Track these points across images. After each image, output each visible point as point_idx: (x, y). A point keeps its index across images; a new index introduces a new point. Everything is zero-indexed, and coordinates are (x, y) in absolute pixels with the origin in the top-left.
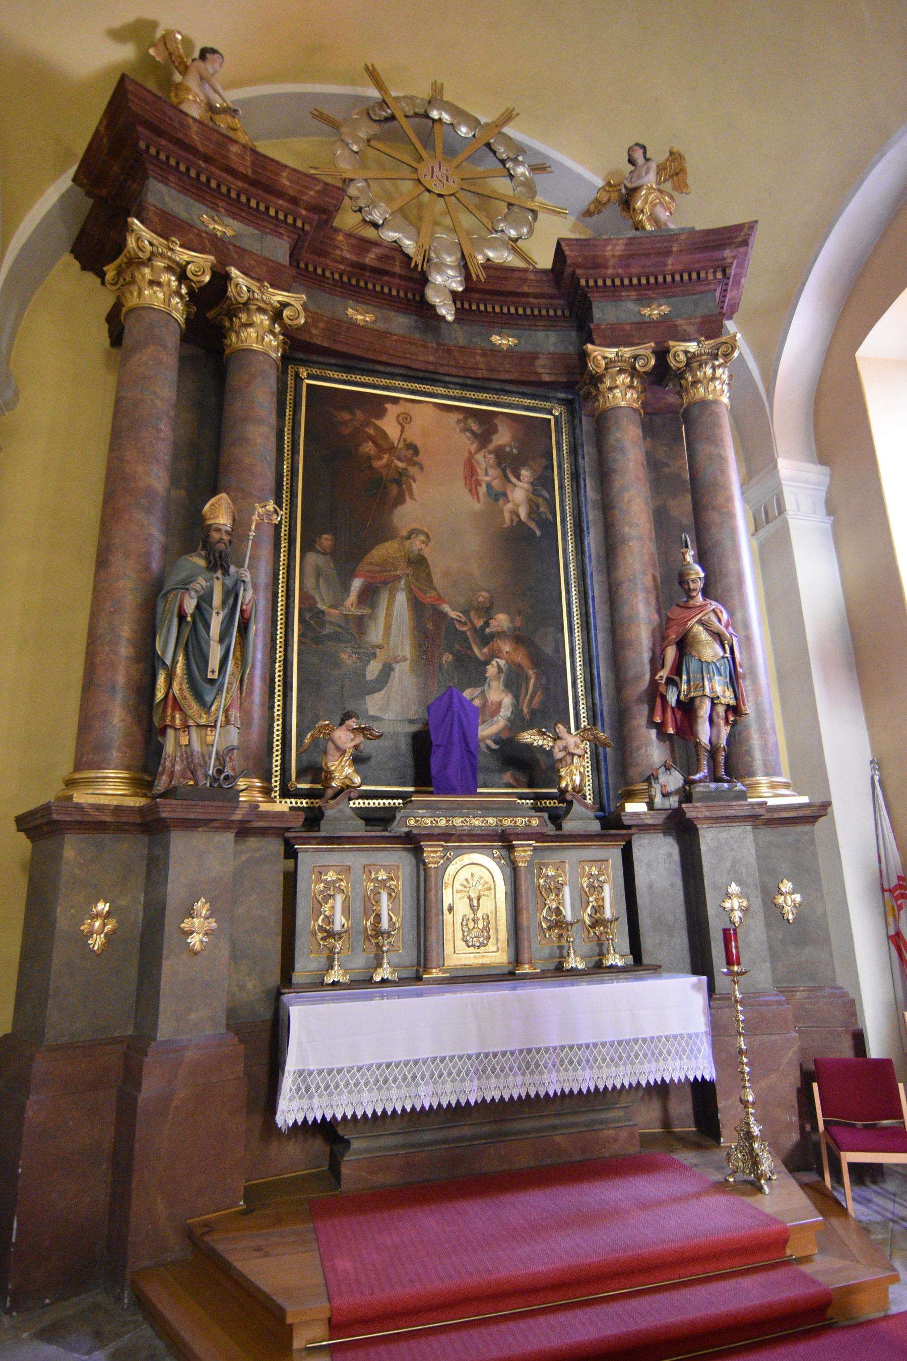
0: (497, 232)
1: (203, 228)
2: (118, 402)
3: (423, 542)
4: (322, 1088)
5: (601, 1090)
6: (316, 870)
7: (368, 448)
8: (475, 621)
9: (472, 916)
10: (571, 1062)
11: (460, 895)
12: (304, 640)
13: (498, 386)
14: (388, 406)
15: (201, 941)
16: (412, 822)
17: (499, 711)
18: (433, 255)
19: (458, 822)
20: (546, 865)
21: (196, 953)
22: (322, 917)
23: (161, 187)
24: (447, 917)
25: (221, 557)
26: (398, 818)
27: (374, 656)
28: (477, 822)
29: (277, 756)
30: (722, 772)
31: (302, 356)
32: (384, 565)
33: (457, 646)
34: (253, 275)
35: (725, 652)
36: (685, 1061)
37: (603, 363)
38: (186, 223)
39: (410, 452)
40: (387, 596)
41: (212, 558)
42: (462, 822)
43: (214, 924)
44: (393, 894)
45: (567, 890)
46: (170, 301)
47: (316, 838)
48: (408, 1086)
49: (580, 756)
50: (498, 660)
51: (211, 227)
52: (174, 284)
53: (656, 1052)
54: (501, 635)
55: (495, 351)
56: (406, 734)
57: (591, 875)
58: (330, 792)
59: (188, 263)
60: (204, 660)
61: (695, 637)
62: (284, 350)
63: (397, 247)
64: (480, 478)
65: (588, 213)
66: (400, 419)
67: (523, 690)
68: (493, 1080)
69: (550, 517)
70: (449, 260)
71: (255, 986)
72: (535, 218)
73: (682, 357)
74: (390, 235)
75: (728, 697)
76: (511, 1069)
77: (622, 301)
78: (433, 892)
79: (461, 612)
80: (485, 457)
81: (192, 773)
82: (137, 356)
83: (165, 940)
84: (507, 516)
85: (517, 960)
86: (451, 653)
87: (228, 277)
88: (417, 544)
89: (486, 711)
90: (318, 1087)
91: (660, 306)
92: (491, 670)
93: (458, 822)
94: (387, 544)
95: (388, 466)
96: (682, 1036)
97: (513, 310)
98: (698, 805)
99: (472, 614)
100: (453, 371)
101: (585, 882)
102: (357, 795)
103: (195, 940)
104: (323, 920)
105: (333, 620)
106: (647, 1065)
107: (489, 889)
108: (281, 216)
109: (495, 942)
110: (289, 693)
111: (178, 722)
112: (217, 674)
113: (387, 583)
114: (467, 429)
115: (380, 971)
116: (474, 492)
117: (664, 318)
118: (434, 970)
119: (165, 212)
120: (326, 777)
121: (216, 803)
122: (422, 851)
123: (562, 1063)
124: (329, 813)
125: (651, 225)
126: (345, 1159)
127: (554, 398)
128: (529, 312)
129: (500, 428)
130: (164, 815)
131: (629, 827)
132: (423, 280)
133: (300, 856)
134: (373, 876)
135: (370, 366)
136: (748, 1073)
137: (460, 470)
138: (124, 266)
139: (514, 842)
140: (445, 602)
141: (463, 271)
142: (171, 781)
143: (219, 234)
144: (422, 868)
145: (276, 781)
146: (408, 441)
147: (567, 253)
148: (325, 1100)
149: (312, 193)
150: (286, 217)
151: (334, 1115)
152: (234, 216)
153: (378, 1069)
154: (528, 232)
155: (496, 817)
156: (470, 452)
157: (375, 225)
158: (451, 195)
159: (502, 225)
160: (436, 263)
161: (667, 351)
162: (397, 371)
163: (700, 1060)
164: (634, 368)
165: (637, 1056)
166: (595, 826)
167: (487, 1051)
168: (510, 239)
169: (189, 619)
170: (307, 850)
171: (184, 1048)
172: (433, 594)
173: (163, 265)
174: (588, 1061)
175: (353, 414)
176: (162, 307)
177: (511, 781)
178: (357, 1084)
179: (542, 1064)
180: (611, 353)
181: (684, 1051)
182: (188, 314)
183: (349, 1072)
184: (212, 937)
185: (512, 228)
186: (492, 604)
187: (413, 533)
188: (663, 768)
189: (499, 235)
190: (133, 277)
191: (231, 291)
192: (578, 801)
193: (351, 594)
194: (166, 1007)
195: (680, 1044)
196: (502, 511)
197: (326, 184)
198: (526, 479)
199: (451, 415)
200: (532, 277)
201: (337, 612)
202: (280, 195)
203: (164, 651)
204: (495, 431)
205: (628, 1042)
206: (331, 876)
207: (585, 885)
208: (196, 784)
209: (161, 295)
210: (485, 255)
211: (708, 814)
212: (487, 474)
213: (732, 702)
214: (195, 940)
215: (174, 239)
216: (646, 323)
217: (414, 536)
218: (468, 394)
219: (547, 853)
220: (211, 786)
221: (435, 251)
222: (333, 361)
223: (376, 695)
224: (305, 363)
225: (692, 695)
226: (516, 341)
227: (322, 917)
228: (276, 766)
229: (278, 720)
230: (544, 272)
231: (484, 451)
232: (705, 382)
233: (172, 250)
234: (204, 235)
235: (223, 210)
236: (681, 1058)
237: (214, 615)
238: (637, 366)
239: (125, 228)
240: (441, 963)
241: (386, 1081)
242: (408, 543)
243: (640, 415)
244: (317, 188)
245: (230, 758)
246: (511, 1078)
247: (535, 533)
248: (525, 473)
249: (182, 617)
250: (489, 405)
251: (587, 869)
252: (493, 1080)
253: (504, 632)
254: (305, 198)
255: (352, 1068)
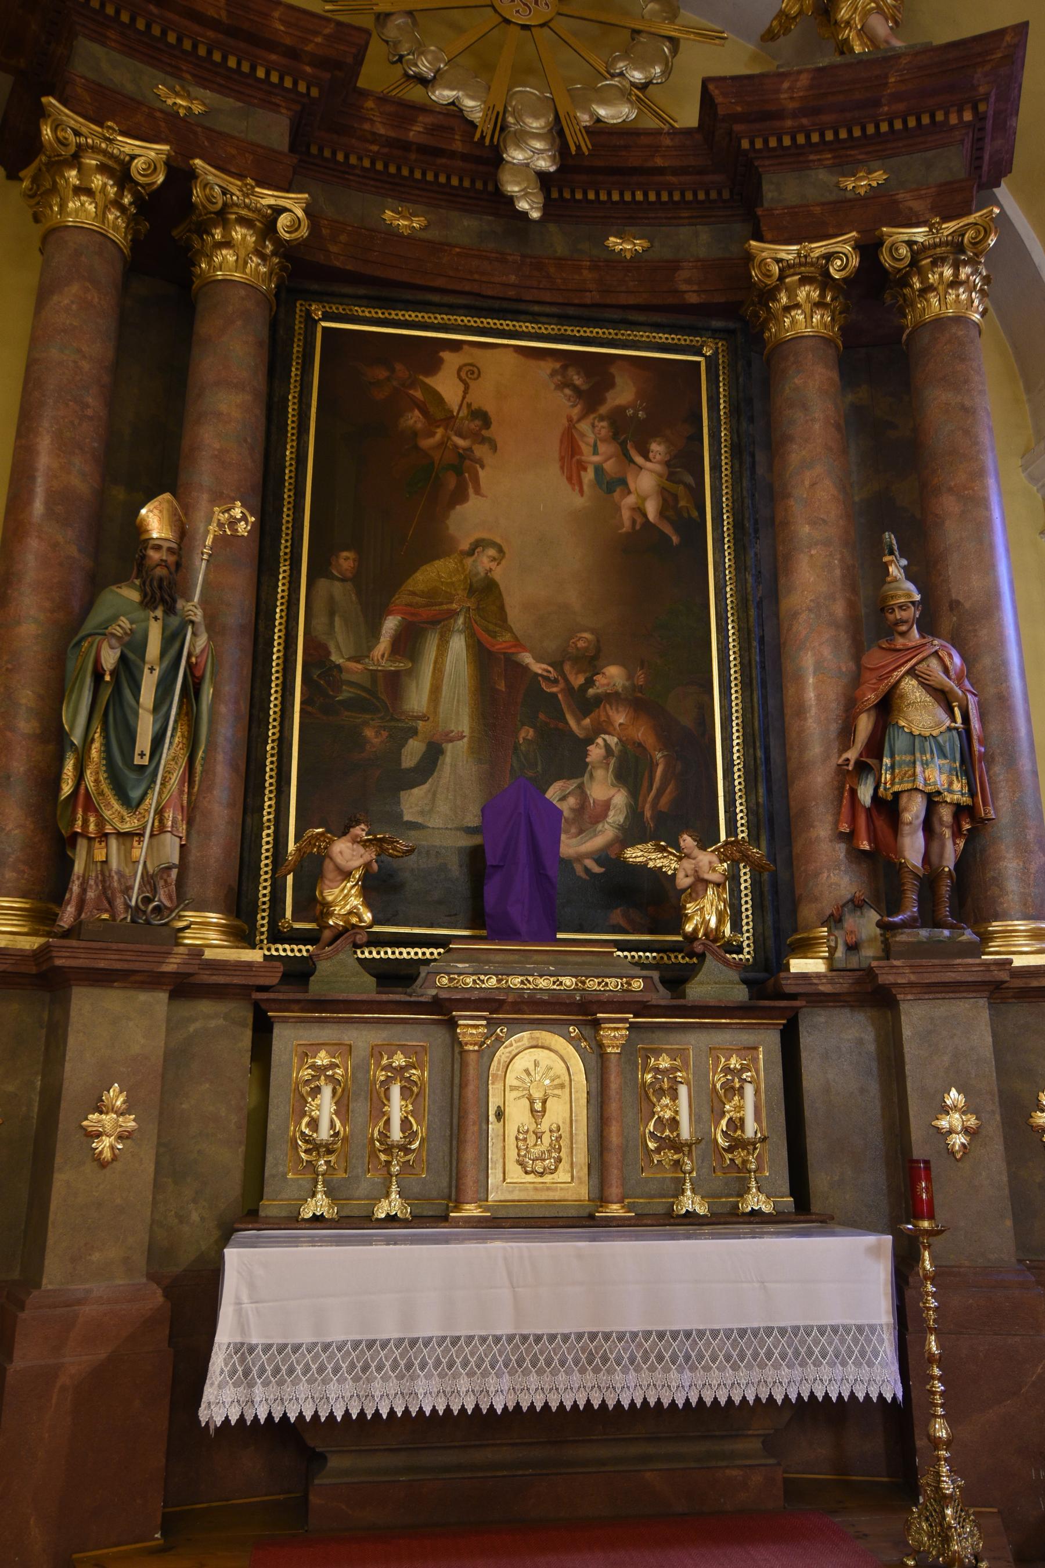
0: (613, 76)
1: (158, 105)
2: (31, 364)
3: (494, 559)
4: (269, 1372)
5: (737, 1403)
6: (300, 1049)
7: (414, 419)
8: (571, 678)
9: (533, 1127)
10: (660, 1358)
11: (515, 1094)
12: (310, 709)
13: (616, 315)
14: (446, 355)
15: (112, 1147)
16: (445, 981)
17: (606, 816)
18: (511, 120)
19: (515, 981)
20: (657, 1053)
21: (103, 1165)
22: (306, 1120)
23: (96, 48)
24: (494, 1126)
25: (160, 587)
26: (423, 975)
27: (414, 732)
28: (543, 983)
29: (266, 880)
30: (945, 911)
31: (315, 287)
32: (432, 596)
33: (542, 716)
34: (233, 170)
35: (954, 720)
36: (851, 1367)
37: (775, 269)
38: (132, 99)
39: (477, 422)
40: (436, 641)
41: (148, 590)
42: (522, 982)
43: (133, 1124)
44: (415, 1089)
45: (683, 1091)
46: (104, 213)
47: (298, 1001)
48: (401, 1377)
49: (718, 885)
50: (606, 737)
51: (170, 102)
52: (112, 191)
53: (803, 1351)
54: (612, 698)
55: (616, 261)
56: (460, 850)
57: (727, 1070)
58: (327, 934)
59: (133, 157)
60: (130, 736)
61: (902, 696)
62: (281, 279)
63: (454, 110)
64: (583, 458)
65: (769, 36)
66: (463, 375)
67: (645, 784)
68: (533, 1377)
69: (695, 514)
70: (536, 124)
71: (202, 1219)
72: (675, 51)
73: (904, 251)
74: (443, 95)
75: (957, 792)
76: (563, 1363)
77: (810, 169)
78: (471, 1087)
79: (549, 665)
80: (593, 426)
81: (110, 903)
82: (55, 298)
83: (59, 1145)
84: (626, 514)
85: (602, 1199)
86: (534, 727)
87: (192, 175)
88: (484, 562)
89: (586, 817)
90: (262, 1371)
91: (870, 172)
92: (595, 752)
93: (515, 981)
94: (438, 564)
95: (442, 444)
96: (847, 1329)
97: (639, 196)
98: (896, 963)
99: (567, 667)
100: (547, 297)
101: (719, 1080)
102: (365, 939)
103: (104, 1145)
104: (308, 1125)
105: (353, 678)
106: (785, 1371)
107: (562, 1086)
108: (274, 78)
109: (568, 1167)
110: (285, 789)
111: (92, 827)
112: (147, 758)
113: (439, 622)
114: (567, 384)
115: (385, 1203)
116: (574, 478)
117: (875, 193)
118: (467, 1207)
119: (100, 85)
120: (322, 912)
121: (138, 947)
122: (457, 1026)
123: (646, 1358)
124: (324, 967)
125: (863, 44)
126: (316, 1482)
127: (707, 329)
128: (665, 197)
129: (618, 380)
130: (58, 962)
131: (793, 997)
132: (495, 160)
133: (277, 1031)
134: (384, 1062)
135: (421, 296)
136: (942, 1394)
137: (553, 448)
138: (44, 169)
139: (599, 1015)
140: (525, 650)
141: (557, 140)
142: (80, 914)
143: (182, 112)
144: (457, 1050)
145: (263, 918)
146: (474, 406)
147: (719, 100)
148: (273, 1391)
149: (319, 40)
150: (281, 79)
151: (285, 1414)
152: (203, 82)
153: (354, 1350)
154: (663, 72)
155: (575, 977)
156: (570, 419)
157: (424, 81)
158: (542, 25)
159: (621, 64)
160: (515, 132)
161: (880, 243)
162: (548, 309)
163: (877, 1369)
164: (827, 274)
165: (769, 1355)
166: (740, 994)
167: (525, 1332)
168: (633, 84)
169: (107, 678)
170: (285, 1020)
171: (79, 1302)
172: (508, 637)
173: (94, 162)
174: (687, 1358)
175: (393, 370)
176: (96, 225)
177: (623, 923)
178: (321, 1369)
179: (612, 1357)
180: (788, 252)
181: (850, 1353)
182: (136, 233)
183: (340, 1351)
184: (129, 1142)
185: (635, 69)
186: (598, 650)
187: (479, 544)
188: (850, 905)
189: (615, 81)
190: (55, 183)
191: (198, 194)
192: (713, 953)
193: (382, 639)
194: (56, 1237)
195: (843, 1341)
196: (618, 509)
197: (339, 24)
198: (658, 457)
199: (542, 364)
200: (668, 142)
201: (360, 666)
202: (272, 46)
203: (72, 727)
204: (612, 385)
205: (755, 1332)
206: (322, 1059)
207: (718, 1086)
208: (113, 917)
209: (91, 208)
210: (593, 114)
211: (913, 978)
212: (595, 452)
213: (966, 800)
214: (104, 1145)
215: (109, 123)
216: (850, 201)
217: (480, 549)
218: (570, 331)
219: (659, 1034)
220: (133, 921)
221: (513, 115)
222: (362, 291)
223: (416, 791)
224: (320, 297)
225: (897, 788)
226: (646, 244)
227: (306, 1120)
228: (264, 895)
229: (269, 828)
230: (688, 132)
231: (592, 416)
232: (941, 288)
233: (110, 141)
234: (158, 114)
235: (189, 77)
236: (844, 1364)
237: (146, 671)
238: (831, 270)
239: (41, 113)
240: (482, 1196)
241: (365, 1368)
242: (469, 561)
243: (837, 347)
244: (327, 31)
245: (166, 881)
246: (562, 1377)
247: (670, 540)
248: (657, 448)
249: (98, 675)
250: (602, 345)
251: (723, 1060)
252: (533, 1377)
253: (616, 694)
254: (309, 48)
255: (315, 1344)
